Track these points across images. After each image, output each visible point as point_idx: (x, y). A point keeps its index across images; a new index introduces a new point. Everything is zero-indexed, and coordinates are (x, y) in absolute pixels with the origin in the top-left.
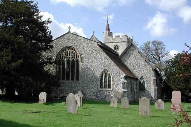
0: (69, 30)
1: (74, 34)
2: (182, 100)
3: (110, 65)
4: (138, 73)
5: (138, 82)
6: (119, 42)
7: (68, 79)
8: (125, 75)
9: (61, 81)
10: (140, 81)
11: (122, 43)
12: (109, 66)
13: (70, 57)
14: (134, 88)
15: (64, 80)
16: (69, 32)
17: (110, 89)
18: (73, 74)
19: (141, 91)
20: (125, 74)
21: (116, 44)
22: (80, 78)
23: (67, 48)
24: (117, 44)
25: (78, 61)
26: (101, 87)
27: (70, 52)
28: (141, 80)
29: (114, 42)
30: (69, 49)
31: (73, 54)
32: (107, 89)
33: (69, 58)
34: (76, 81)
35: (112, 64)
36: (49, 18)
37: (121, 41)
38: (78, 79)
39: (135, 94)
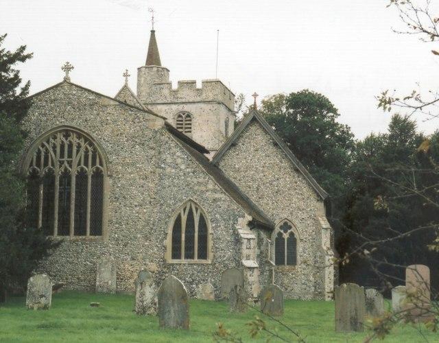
0: (63, 74)
1: (154, 104)
2: (343, 275)
3: (204, 189)
4: (276, 212)
5: (275, 235)
6: (194, 102)
7: (80, 231)
8: (250, 218)
9: (56, 237)
10: (280, 234)
11: (202, 105)
12: (202, 192)
13: (70, 163)
14: (266, 257)
15: (85, 234)
16: (66, 80)
17: (203, 261)
18: (190, 239)
19: (284, 264)
20: (250, 214)
21: (180, 107)
22: (106, 227)
23: (60, 131)
24: (187, 108)
25: (98, 176)
26: (176, 255)
27: (70, 146)
28: (282, 231)
29: (175, 103)
30: (67, 136)
31: (82, 153)
32: (196, 260)
33: (66, 164)
34: (92, 237)
35: (210, 186)
36: (6, 35)
37: (198, 99)
38: (97, 230)
39: (271, 276)
